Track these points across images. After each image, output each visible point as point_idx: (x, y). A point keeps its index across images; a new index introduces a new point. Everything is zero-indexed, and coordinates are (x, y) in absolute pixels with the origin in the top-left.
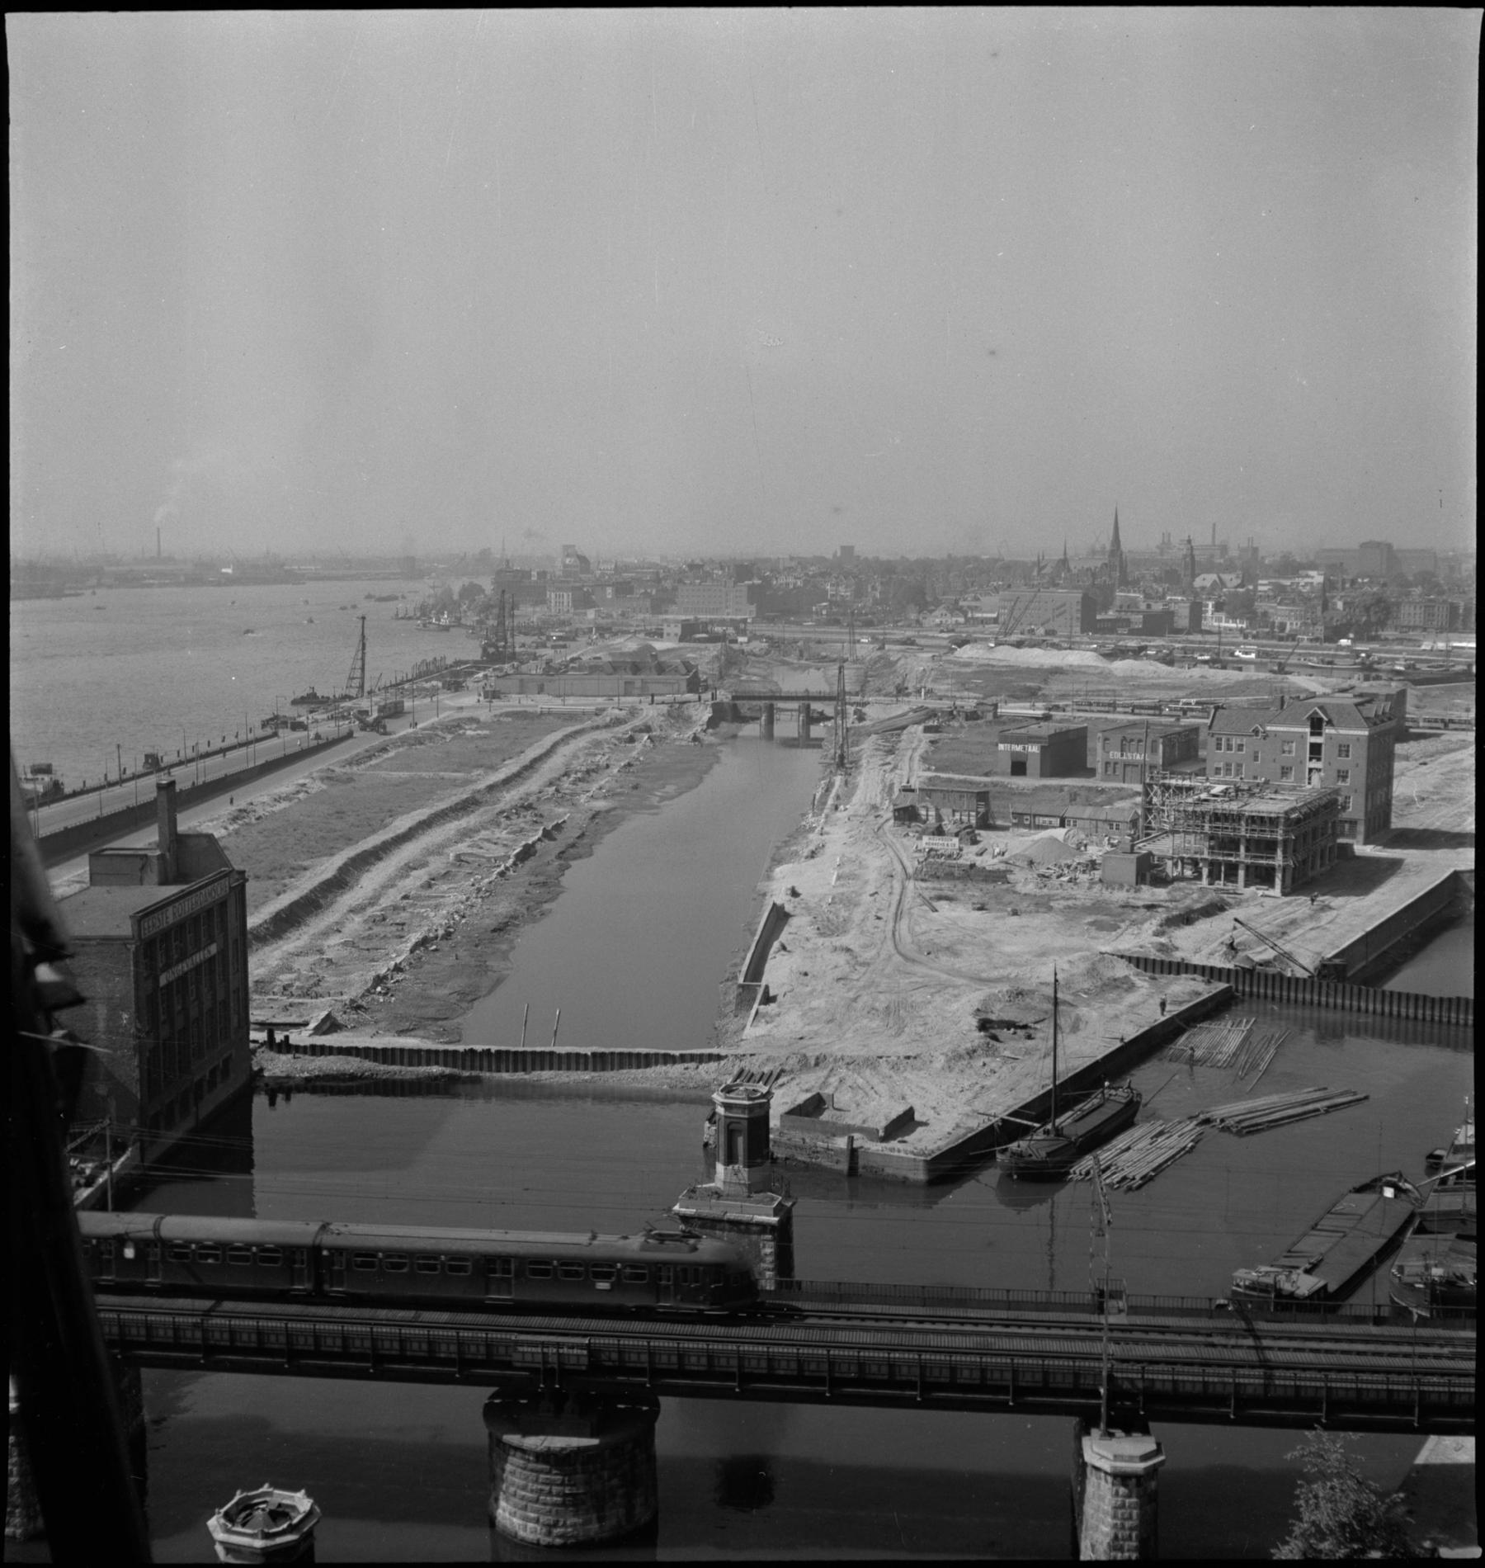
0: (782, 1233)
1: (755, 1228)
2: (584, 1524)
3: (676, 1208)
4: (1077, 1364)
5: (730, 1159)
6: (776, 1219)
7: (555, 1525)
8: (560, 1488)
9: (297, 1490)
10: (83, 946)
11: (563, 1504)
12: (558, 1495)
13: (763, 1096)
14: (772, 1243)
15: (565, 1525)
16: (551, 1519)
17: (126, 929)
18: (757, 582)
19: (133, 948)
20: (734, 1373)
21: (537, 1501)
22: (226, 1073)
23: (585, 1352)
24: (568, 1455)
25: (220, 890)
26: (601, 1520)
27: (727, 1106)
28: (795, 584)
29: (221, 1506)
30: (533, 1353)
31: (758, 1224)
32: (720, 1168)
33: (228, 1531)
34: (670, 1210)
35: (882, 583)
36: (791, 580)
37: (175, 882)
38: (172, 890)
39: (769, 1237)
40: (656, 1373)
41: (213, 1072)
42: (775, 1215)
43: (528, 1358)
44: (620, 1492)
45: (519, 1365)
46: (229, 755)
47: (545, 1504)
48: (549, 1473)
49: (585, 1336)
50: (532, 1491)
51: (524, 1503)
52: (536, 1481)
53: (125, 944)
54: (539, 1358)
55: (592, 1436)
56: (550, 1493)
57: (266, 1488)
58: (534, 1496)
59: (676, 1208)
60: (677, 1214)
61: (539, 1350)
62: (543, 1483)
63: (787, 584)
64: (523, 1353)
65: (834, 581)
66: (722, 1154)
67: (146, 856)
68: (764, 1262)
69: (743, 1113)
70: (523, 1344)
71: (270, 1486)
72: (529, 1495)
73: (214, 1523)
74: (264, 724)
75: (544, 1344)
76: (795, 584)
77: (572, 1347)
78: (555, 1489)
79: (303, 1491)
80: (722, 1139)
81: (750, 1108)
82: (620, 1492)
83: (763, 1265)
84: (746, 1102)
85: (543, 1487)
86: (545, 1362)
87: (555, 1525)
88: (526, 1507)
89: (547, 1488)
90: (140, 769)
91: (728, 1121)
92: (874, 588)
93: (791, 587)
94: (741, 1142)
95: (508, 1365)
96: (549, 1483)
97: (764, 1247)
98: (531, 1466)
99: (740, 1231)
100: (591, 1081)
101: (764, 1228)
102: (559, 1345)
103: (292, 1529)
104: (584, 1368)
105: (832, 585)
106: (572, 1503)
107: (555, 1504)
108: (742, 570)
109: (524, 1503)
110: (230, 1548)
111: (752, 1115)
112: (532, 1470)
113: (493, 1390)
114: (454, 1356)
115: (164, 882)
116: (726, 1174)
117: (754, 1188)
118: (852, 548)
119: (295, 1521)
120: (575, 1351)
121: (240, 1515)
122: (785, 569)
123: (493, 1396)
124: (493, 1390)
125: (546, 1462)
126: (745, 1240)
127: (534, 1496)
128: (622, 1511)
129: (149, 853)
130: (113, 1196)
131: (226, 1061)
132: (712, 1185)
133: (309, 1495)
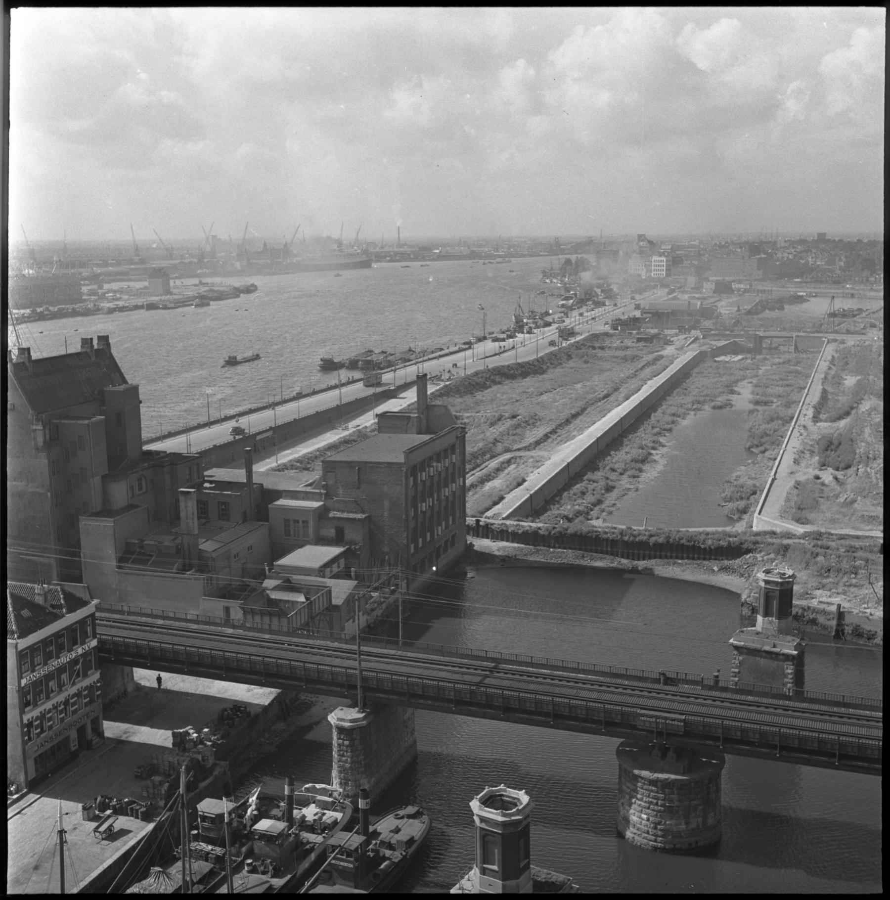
0: (798, 661)
1: (781, 657)
2: (677, 825)
3: (731, 641)
4: (861, 741)
5: (766, 614)
6: (796, 652)
7: (659, 823)
8: (663, 802)
9: (520, 790)
10: (377, 467)
11: (664, 811)
12: (661, 806)
13: (790, 577)
14: (792, 667)
15: (665, 824)
16: (657, 820)
17: (401, 459)
18: (763, 256)
19: (404, 469)
20: (776, 745)
21: (649, 808)
22: (453, 544)
23: (682, 724)
24: (669, 783)
25: (451, 439)
26: (687, 823)
27: (767, 582)
28: (788, 258)
29: (477, 795)
30: (649, 722)
31: (783, 654)
32: (760, 618)
33: (481, 809)
34: (726, 642)
35: (846, 257)
36: (786, 255)
37: (426, 433)
38: (426, 437)
39: (791, 663)
40: (727, 740)
41: (446, 542)
42: (795, 650)
43: (647, 724)
44: (701, 807)
45: (640, 727)
46: (502, 355)
47: (653, 810)
48: (657, 792)
49: (683, 714)
50: (645, 802)
51: (655, 813)
52: (649, 796)
53: (401, 467)
54: (654, 725)
55: (683, 774)
56: (657, 804)
57: (502, 786)
58: (647, 805)
59: (731, 641)
60: (732, 644)
61: (654, 720)
62: (653, 798)
63: (783, 257)
64: (644, 721)
65: (814, 255)
66: (761, 610)
67: (410, 416)
68: (787, 678)
69: (777, 586)
70: (643, 715)
71: (505, 786)
72: (643, 804)
73: (475, 805)
74: (465, 344)
75: (657, 717)
76: (788, 258)
77: (674, 720)
78: (660, 802)
79: (524, 791)
80: (762, 601)
81: (782, 584)
82: (701, 807)
83: (786, 680)
84: (780, 580)
85: (653, 800)
86: (657, 727)
87: (659, 823)
88: (642, 810)
89: (655, 801)
90: (844, 331)
91: (767, 590)
92: (840, 260)
93: (786, 259)
94: (775, 604)
95: (635, 727)
96: (657, 799)
97: (787, 668)
98: (645, 787)
99: (772, 658)
100: (596, 559)
101: (787, 657)
102: (666, 718)
103: (519, 812)
104: (681, 733)
105: (812, 258)
106: (669, 811)
107: (659, 811)
108: (755, 248)
109: (655, 813)
110: (483, 819)
111: (782, 588)
112: (646, 790)
113: (621, 740)
114: (452, 698)
115: (419, 433)
116: (763, 623)
117: (782, 631)
118: (825, 234)
119: (520, 807)
120: (676, 723)
121: (490, 801)
122: (781, 248)
123: (622, 744)
124: (621, 740)
125: (656, 786)
126: (775, 664)
127: (647, 805)
128: (700, 820)
129: (412, 415)
130: (402, 610)
131: (453, 537)
132: (754, 628)
133: (526, 793)
